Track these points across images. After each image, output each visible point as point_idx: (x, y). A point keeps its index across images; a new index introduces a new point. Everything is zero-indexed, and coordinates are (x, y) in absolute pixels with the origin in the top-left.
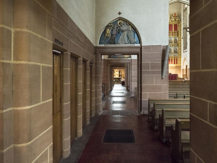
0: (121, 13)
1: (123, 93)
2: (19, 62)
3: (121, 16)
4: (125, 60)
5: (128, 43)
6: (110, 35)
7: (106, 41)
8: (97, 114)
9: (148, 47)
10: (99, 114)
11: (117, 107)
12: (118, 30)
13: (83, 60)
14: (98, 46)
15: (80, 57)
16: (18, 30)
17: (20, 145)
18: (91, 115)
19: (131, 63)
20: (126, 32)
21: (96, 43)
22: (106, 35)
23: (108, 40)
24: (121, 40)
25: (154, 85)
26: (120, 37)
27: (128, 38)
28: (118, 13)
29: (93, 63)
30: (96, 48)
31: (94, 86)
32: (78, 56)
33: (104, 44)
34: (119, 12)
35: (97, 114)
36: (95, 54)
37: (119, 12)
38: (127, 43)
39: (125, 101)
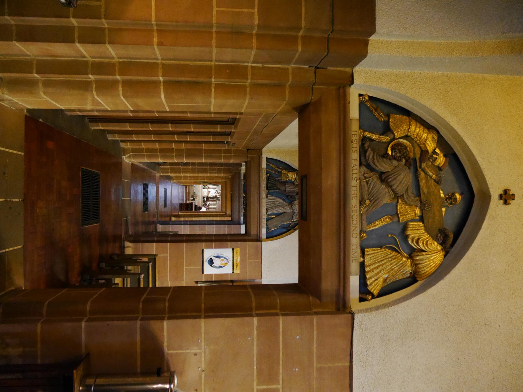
0: (502, 202)
1: (165, 205)
2: (213, 90)
3: (495, 203)
4: (239, 209)
5: (268, 215)
6: (283, 179)
7: (273, 172)
8: (124, 151)
9: (258, 254)
10: (124, 157)
11: (136, 193)
12: (294, 194)
13: (236, 118)
14: (263, 155)
15: (235, 128)
16: (248, 89)
17: (120, 89)
18: (110, 132)
19: (247, 238)
20: (290, 211)
21: (269, 152)
22: (284, 172)
23: (274, 176)
24: (274, 202)
25: (185, 267)
26: (280, 198)
27: (278, 215)
28: (506, 191)
29: (229, 145)
30: (259, 152)
31: (183, 146)
32: (237, 126)
33: (267, 168)
34: (513, 195)
35: (124, 151)
36: (248, 150)
37: (513, 195)
38: (268, 213)
39: (148, 211)
